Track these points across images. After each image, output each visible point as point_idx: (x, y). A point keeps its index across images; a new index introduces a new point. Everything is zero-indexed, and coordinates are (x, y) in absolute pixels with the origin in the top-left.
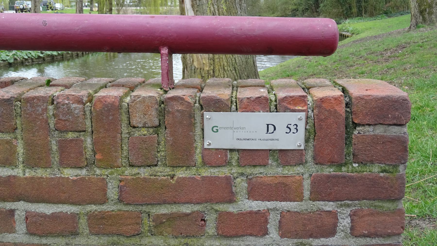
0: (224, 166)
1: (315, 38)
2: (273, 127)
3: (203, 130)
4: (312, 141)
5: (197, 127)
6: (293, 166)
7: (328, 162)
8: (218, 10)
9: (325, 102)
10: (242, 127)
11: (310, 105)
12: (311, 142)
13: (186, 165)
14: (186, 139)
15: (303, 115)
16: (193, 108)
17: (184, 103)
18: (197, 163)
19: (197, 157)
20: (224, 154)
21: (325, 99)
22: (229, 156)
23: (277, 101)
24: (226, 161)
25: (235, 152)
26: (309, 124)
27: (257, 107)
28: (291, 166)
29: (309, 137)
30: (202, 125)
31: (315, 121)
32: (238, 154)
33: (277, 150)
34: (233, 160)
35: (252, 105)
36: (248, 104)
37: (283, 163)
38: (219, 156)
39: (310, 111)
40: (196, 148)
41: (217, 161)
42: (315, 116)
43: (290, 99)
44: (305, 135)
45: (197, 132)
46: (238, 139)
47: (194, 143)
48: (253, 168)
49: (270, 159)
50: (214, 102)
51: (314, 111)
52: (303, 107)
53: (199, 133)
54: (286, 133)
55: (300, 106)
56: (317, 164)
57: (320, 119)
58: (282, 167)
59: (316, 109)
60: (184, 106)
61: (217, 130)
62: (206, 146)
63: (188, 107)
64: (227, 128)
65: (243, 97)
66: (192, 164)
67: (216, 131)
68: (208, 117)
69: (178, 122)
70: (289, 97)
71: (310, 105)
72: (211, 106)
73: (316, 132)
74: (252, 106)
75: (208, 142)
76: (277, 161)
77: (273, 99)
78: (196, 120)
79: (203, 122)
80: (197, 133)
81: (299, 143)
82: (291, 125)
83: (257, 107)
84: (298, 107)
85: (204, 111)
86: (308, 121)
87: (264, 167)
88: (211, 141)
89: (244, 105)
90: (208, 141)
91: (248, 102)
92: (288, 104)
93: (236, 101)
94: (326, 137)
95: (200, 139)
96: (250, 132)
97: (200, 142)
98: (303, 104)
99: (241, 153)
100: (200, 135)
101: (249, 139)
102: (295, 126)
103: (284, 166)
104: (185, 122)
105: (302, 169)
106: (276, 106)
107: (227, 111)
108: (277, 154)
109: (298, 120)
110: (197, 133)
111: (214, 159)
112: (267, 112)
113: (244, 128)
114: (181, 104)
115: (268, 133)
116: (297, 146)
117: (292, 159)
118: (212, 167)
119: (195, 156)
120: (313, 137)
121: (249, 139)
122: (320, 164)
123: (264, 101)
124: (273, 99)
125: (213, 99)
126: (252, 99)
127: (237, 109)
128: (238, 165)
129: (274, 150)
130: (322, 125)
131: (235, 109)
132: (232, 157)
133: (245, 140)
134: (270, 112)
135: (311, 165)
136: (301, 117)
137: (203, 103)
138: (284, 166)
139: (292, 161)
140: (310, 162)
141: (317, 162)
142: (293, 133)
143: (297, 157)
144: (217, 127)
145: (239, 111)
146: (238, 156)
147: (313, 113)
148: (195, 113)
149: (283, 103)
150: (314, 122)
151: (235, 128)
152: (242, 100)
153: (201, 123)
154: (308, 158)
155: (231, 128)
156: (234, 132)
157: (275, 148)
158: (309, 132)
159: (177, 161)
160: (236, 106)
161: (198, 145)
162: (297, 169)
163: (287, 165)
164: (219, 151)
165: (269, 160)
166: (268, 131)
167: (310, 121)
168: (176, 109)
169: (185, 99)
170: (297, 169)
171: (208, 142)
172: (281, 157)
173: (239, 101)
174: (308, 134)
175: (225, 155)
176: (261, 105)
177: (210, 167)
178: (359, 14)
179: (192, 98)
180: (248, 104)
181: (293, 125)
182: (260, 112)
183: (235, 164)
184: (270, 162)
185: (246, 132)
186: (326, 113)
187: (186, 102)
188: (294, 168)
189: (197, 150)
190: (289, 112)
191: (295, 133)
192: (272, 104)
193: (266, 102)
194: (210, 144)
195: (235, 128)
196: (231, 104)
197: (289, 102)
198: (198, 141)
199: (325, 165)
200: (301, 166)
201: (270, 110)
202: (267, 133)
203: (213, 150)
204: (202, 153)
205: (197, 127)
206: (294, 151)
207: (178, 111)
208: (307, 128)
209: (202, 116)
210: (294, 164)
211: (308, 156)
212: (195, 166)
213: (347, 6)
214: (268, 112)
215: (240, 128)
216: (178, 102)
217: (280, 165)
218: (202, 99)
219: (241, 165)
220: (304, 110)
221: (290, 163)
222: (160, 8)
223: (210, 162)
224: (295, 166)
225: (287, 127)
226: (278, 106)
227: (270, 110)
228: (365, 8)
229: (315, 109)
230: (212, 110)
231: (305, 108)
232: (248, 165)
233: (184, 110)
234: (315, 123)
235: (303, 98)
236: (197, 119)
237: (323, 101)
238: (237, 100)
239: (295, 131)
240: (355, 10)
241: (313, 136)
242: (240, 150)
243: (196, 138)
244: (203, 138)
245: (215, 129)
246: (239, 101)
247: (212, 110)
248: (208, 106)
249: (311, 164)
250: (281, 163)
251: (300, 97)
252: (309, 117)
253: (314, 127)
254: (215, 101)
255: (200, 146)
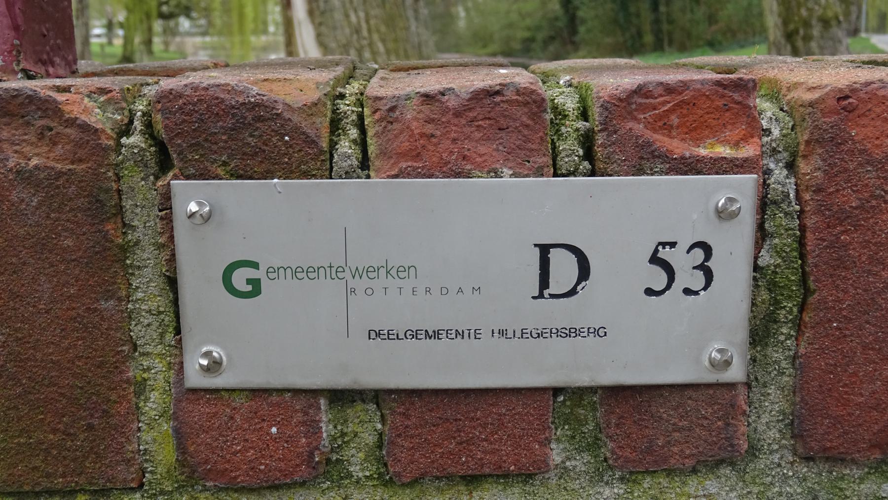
0: (303, 484)
1: (597, 61)
2: (572, 259)
3: (172, 283)
4: (789, 337)
5: (139, 268)
6: (682, 472)
7: (873, 447)
8: (367, 22)
9: (864, 115)
10: (394, 263)
11: (776, 132)
12: (782, 338)
13: (91, 484)
14: (78, 339)
15: (748, 181)
16: (113, 156)
17: (60, 129)
18: (151, 472)
19: (146, 436)
20: (299, 417)
21: (862, 95)
22: (327, 429)
23: (595, 112)
24: (311, 455)
25: (359, 406)
26: (777, 241)
27: (482, 149)
28: (670, 473)
29: (773, 312)
30: (165, 255)
31: (809, 222)
32: (377, 418)
33: (592, 390)
34: (353, 451)
35: (453, 135)
36: (429, 129)
37: (627, 460)
38: (274, 430)
39: (772, 166)
40: (141, 388)
41: (263, 456)
42: (807, 196)
43: (667, 98)
44: (753, 304)
45: (140, 295)
46: (378, 334)
47: (128, 358)
48: (462, 488)
49: (558, 440)
50: (230, 122)
51: (803, 167)
52: (736, 145)
53: (153, 305)
54: (649, 292)
55: (725, 142)
56: (808, 459)
57: (835, 208)
58: (622, 479)
59: (811, 153)
60: (59, 150)
61: (255, 283)
62: (194, 378)
63: (81, 153)
64: (312, 272)
65: (402, 93)
66: (121, 477)
67: (249, 288)
68: (193, 207)
69: (28, 243)
70: (660, 90)
71: (776, 132)
72: (215, 147)
73: (812, 286)
74: (454, 140)
75: (207, 354)
76: (594, 446)
77: (570, 104)
78: (134, 228)
79: (172, 237)
80: (142, 300)
81: (720, 351)
82: (673, 245)
83: (482, 149)
84: (712, 146)
85: (175, 177)
86: (767, 225)
87: (525, 482)
88: (224, 348)
89: (404, 137)
90: (204, 349)
91: (429, 121)
92: (654, 130)
93: (361, 117)
94: (866, 313)
95: (162, 335)
96: (444, 291)
97: (161, 355)
98: (740, 130)
99: (393, 412)
100: (160, 313)
101: (436, 335)
102: (699, 255)
103: (631, 473)
104: (69, 242)
105: (731, 490)
106: (587, 141)
107: (306, 175)
108: (595, 409)
109: (716, 220)
110: (142, 300)
111: (246, 450)
112: (539, 172)
113: (404, 271)
114: (41, 136)
115: (546, 293)
116: (707, 363)
117: (676, 435)
118: (236, 491)
119: (139, 429)
120: (790, 312)
121: (436, 335)
122: (827, 459)
123: (521, 115)
124: (570, 104)
125: (223, 101)
126: (452, 102)
127: (365, 164)
128: (381, 475)
129: (580, 389)
130: (845, 246)
131: (356, 163)
132: (343, 434)
133: (415, 335)
134: (555, 175)
135: (779, 465)
136: (731, 200)
137: (166, 127)
138: (631, 473)
139: (675, 449)
140: (776, 447)
141: (812, 449)
142: (687, 291)
143: (705, 423)
144: (255, 265)
145: (378, 171)
146: (379, 426)
147: (793, 180)
148: (124, 188)
149: (630, 125)
150: (802, 228)
151: (357, 273)
152: (392, 109)
153: (160, 247)
154: (761, 428)
155: (335, 272)
156: (353, 291)
157: (583, 379)
158: (772, 286)
159: (37, 462)
160: (363, 144)
161: (149, 369)
162: (704, 489)
163: (647, 472)
164: (271, 405)
165: (553, 446)
166: (544, 282)
167: (778, 221)
168: (11, 164)
169: (67, 108)
170: (704, 489)
171: (207, 354)
172: (617, 425)
173: (377, 116)
174: (765, 295)
175: (304, 423)
176: (503, 134)
177: (227, 489)
178: (658, 47)
179: (108, 101)
180: (429, 129)
181: (684, 244)
182: (497, 174)
183: (362, 470)
184: (556, 454)
185: (421, 290)
186: (870, 176)
187: (72, 122)
188: (684, 483)
189: (147, 400)
190: (661, 173)
191: (696, 293)
192: (563, 129)
193: (529, 122)
194: (214, 366)
195: (357, 273)
196: (332, 133)
197: (660, 117)
198: (149, 349)
199: (854, 461)
200: (726, 471)
201: (554, 165)
202: (541, 296)
203: (239, 401)
204: (175, 417)
205: (139, 268)
206: (689, 393)
207: (24, 176)
208: (760, 262)
209: (166, 202)
210: (689, 463)
211: (765, 419)
212: (141, 485)
213: (634, 30)
214: (542, 175)
215: (383, 272)
216: (28, 124)
217: (610, 467)
218: (159, 106)
219: (398, 475)
220: (746, 160)
221: (665, 460)
222: (253, 39)
223: (220, 467)
224: (694, 471)
225: (655, 259)
226: (600, 139)
227: (554, 165)
228: (670, 34)
229: (805, 157)
230: (220, 171)
231: (748, 151)
232: (436, 472)
233: (60, 174)
234: (809, 235)
235: (737, 96)
236: (136, 223)
237: (849, 110)
238: (367, 111)
239: (697, 280)
240: (649, 38)
241: (795, 310)
242: (390, 392)
243: (136, 331)
244: (178, 331)
245: (240, 279)
246: (377, 116)
247: (220, 171)
248: (198, 144)
249: (776, 458)
250: (616, 460)
251: (720, 90)
252: (775, 203)
253: (802, 256)
254: (234, 115)
255: (160, 377)
